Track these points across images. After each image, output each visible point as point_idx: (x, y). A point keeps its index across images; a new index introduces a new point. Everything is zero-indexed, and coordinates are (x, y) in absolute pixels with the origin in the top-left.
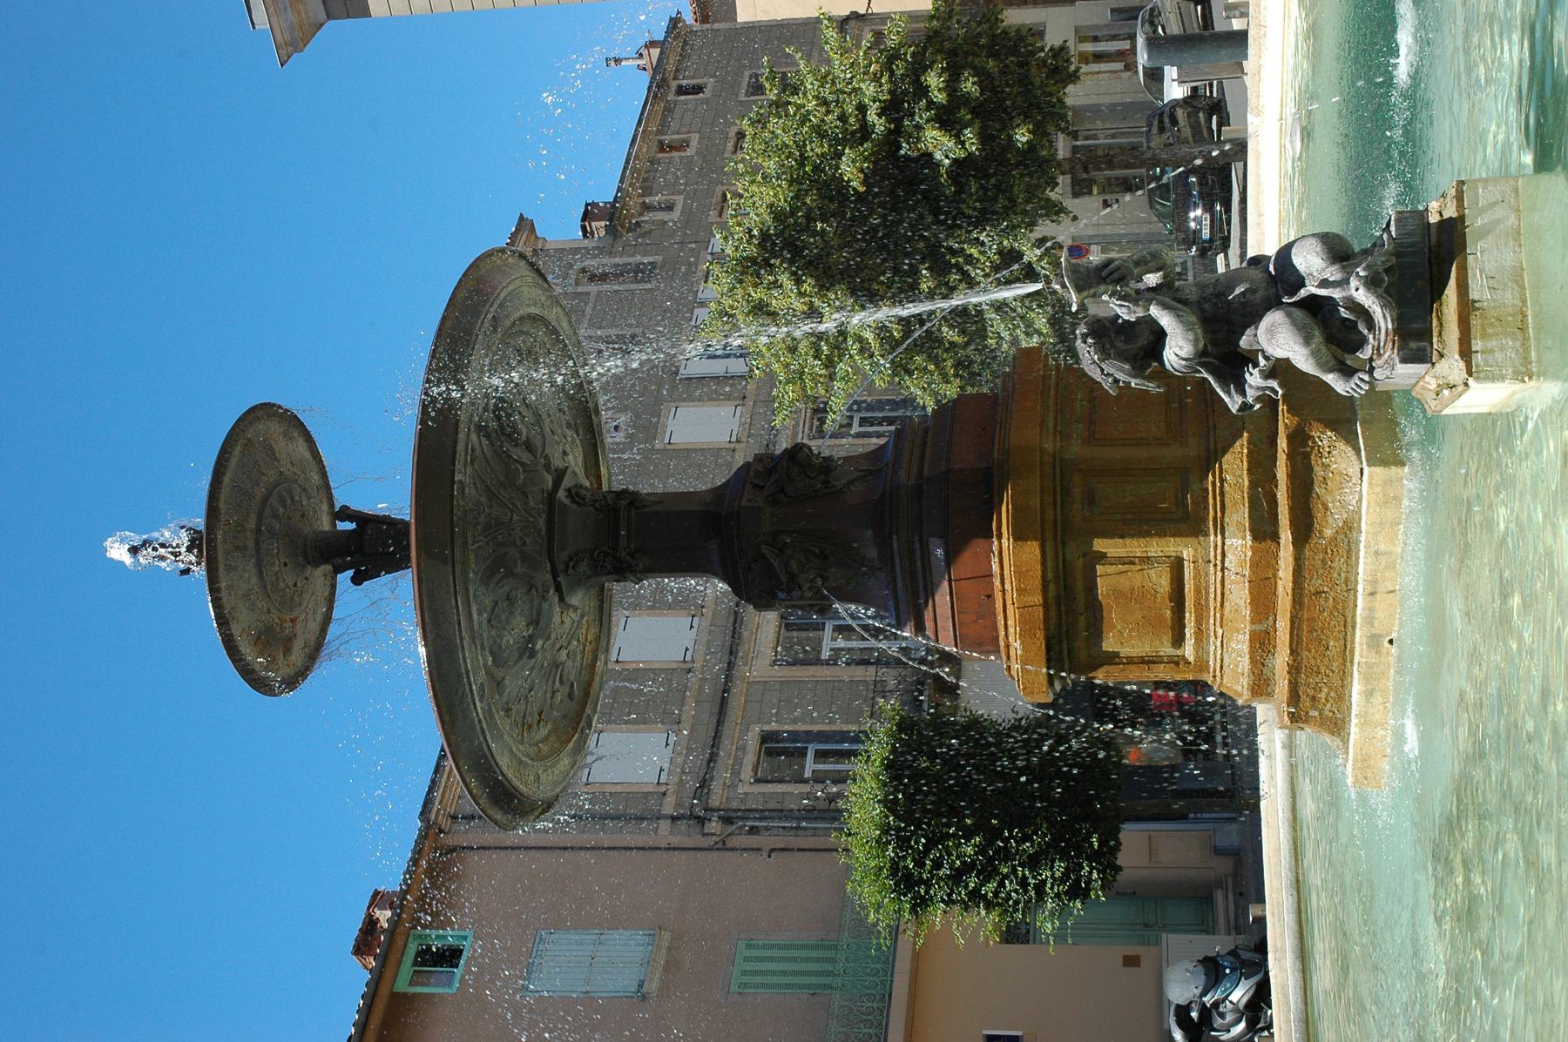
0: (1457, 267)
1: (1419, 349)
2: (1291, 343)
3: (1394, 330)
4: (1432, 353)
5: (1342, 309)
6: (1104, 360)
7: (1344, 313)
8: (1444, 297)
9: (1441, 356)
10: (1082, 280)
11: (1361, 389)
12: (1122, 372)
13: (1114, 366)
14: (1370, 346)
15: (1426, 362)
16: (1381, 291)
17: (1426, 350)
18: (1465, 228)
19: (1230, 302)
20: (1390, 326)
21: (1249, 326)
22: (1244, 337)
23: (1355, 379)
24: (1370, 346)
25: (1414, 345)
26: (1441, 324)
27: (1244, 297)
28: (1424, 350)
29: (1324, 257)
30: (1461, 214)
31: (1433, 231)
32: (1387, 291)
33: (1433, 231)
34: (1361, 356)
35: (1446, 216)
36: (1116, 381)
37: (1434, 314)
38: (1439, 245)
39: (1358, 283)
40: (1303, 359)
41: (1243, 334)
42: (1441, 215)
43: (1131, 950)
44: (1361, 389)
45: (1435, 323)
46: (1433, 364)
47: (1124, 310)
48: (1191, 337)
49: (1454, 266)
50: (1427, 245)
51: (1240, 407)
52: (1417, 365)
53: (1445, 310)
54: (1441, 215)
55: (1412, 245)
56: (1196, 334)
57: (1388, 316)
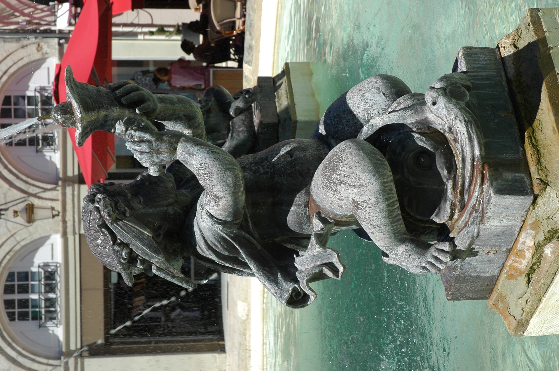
0: (547, 86)
1: (515, 180)
2: (358, 171)
3: (482, 157)
4: (532, 185)
5: (416, 135)
6: (116, 220)
7: (421, 142)
8: (536, 123)
9: (545, 184)
10: (90, 98)
11: (441, 261)
12: (141, 240)
13: (130, 230)
14: (448, 203)
15: (527, 194)
16: (463, 104)
17: (524, 182)
18: (549, 49)
19: (274, 165)
20: (477, 153)
21: (299, 191)
22: (293, 208)
23: (433, 252)
24: (448, 203)
25: (508, 176)
26: (538, 151)
27: (291, 156)
28: (522, 181)
29: (386, 92)
30: (541, 36)
31: (510, 64)
32: (468, 105)
33: (510, 64)
34: (437, 221)
35: (522, 45)
36: (132, 259)
37: (527, 142)
38: (519, 74)
39: (435, 95)
40: (373, 201)
41: (291, 205)
42: (515, 46)
43: (453, 143)
44: (441, 261)
45: (529, 151)
46: (536, 198)
47: (144, 147)
48: (230, 180)
49: (544, 85)
50: (504, 79)
51: (291, 296)
52: (518, 197)
53: (539, 136)
54: (515, 46)
55: (488, 78)
56: (236, 177)
57: (474, 137)
